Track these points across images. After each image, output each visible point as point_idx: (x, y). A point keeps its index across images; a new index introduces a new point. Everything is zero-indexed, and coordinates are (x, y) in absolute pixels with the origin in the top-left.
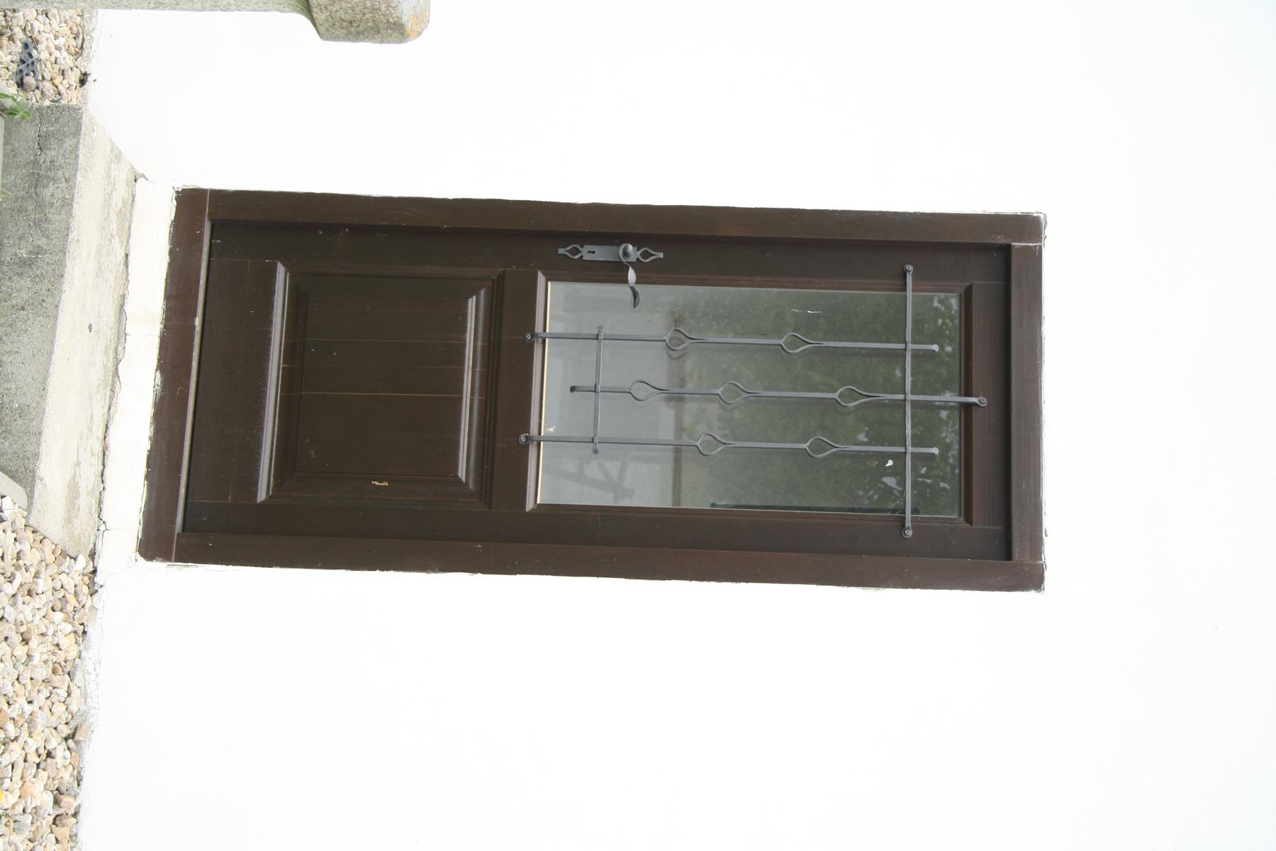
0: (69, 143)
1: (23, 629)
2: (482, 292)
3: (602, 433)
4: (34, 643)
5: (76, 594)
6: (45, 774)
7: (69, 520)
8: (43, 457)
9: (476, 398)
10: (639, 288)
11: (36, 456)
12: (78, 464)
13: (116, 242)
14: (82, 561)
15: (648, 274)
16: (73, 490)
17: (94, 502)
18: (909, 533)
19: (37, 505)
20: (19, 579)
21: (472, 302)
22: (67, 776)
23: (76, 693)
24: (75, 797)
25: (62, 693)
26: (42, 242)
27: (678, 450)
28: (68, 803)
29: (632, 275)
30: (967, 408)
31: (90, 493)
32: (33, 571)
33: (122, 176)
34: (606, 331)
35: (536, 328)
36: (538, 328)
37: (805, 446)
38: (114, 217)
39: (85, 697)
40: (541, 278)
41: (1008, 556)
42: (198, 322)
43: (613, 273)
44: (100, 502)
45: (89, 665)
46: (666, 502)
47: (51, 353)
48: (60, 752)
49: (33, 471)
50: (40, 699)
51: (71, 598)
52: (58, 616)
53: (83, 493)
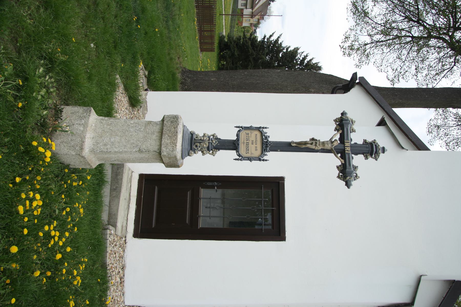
0: (122, 169)
1: (115, 252)
2: (190, 191)
3: (211, 215)
4: (117, 254)
5: (123, 244)
6: (119, 275)
7: (122, 232)
8: (118, 222)
9: (190, 209)
10: (217, 190)
11: (117, 222)
12: (123, 222)
13: (129, 184)
14: (124, 238)
15: (219, 187)
16: (122, 226)
17: (126, 228)
18: (263, 231)
19: (117, 231)
20: (114, 244)
21: (189, 192)
22: (122, 275)
23: (123, 261)
24: (123, 279)
25: (121, 261)
26: (117, 186)
27: (224, 218)
28: (122, 280)
29: (216, 188)
30: (273, 209)
31: (125, 227)
32: (116, 242)
33: (130, 172)
34: (212, 197)
35: (215, 226)
36: (200, 197)
37: (246, 217)
38: (129, 180)
39: (125, 261)
40: (200, 188)
41: (280, 235)
42: (142, 196)
43: (213, 187)
44: (127, 228)
45: (125, 256)
46: (222, 227)
47: (119, 205)
48: (121, 272)
49: (116, 225)
50: (118, 263)
51: (122, 245)
52: (120, 248)
53: (124, 227)
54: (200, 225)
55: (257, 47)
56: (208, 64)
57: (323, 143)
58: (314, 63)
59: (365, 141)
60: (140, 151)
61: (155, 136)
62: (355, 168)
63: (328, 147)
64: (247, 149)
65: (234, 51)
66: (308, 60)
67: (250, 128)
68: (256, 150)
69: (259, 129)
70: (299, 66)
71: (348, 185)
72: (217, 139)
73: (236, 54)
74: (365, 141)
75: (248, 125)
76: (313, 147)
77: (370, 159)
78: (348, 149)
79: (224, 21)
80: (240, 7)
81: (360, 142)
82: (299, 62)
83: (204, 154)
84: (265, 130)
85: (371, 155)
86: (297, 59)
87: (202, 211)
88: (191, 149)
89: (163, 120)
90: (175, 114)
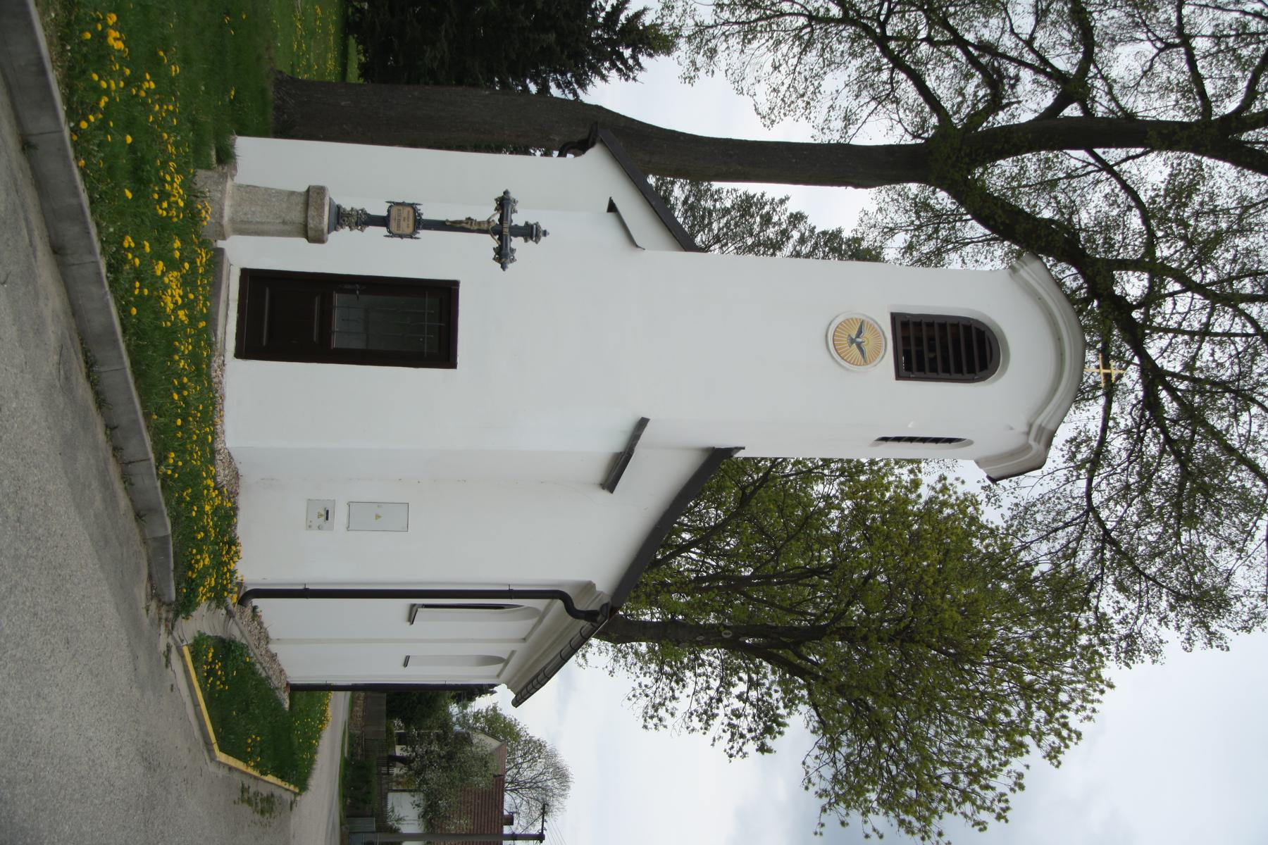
43: (353, 292)
54: (334, 345)
56: (316, 20)
57: (479, 223)
58: (647, 24)
59: (527, 223)
60: (284, 223)
61: (300, 208)
62: (513, 250)
63: (485, 227)
64: (399, 226)
66: (631, 14)
67: (403, 204)
68: (407, 227)
69: (412, 206)
70: (603, 30)
71: (504, 267)
72: (366, 214)
74: (527, 223)
75: (401, 201)
76: (468, 226)
77: (531, 243)
78: (506, 231)
81: (522, 224)
82: (600, 20)
83: (351, 229)
84: (418, 207)
85: (532, 238)
86: (596, 8)
87: (336, 325)
88: (338, 223)
89: (308, 191)
90: (320, 183)
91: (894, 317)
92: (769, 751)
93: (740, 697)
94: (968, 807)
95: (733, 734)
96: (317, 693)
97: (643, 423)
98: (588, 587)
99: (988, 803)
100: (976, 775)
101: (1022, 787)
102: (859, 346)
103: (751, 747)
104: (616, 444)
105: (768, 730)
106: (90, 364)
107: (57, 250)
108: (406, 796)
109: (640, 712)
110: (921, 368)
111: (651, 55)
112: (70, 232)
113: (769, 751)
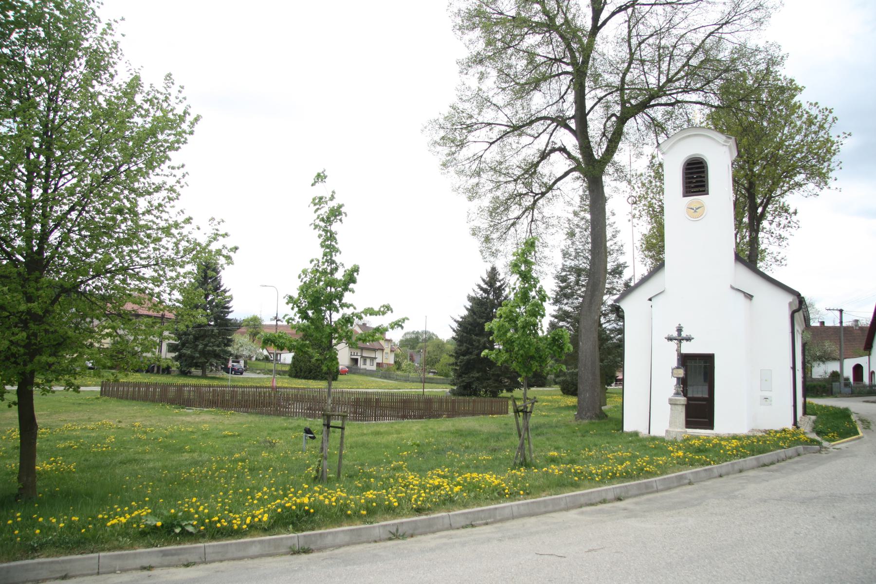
55: (468, 349)
61: (676, 406)
65: (473, 377)
73: (477, 375)
78: (680, 338)
79: (401, 390)
80: (374, 368)
87: (700, 395)
91: (684, 196)
92: (796, 210)
93: (771, 224)
94: (826, 126)
95: (789, 227)
96: (807, 405)
97: (732, 288)
98: (790, 304)
99: (824, 117)
100: (810, 122)
101: (816, 103)
102: (697, 209)
103: (794, 218)
104: (741, 296)
105: (786, 211)
106: (765, 465)
107: (741, 471)
108: (814, 370)
109: (779, 268)
110: (703, 186)
111: (499, 275)
112: (737, 467)
113: (796, 210)
